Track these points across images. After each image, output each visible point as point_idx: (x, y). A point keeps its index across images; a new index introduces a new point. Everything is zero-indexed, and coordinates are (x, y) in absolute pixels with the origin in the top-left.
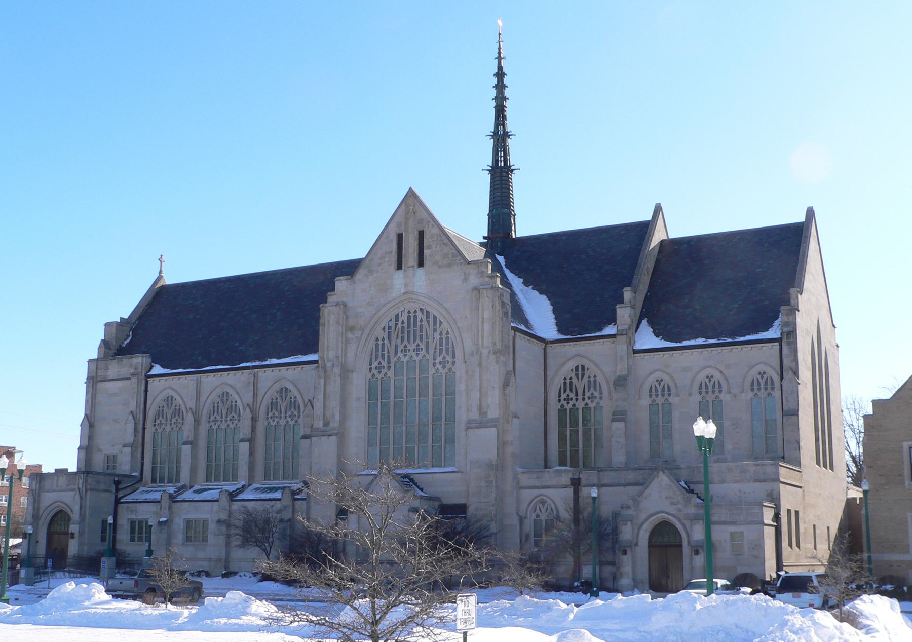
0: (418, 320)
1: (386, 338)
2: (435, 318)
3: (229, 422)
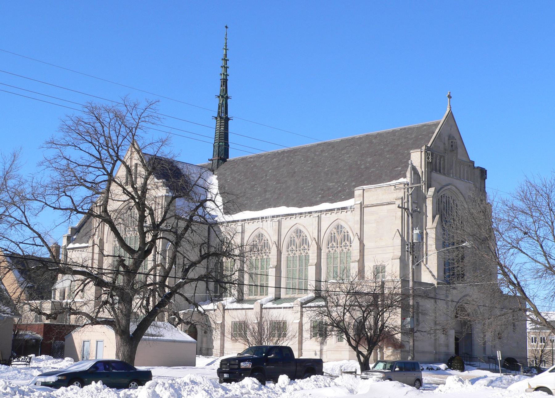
3: (343, 248)
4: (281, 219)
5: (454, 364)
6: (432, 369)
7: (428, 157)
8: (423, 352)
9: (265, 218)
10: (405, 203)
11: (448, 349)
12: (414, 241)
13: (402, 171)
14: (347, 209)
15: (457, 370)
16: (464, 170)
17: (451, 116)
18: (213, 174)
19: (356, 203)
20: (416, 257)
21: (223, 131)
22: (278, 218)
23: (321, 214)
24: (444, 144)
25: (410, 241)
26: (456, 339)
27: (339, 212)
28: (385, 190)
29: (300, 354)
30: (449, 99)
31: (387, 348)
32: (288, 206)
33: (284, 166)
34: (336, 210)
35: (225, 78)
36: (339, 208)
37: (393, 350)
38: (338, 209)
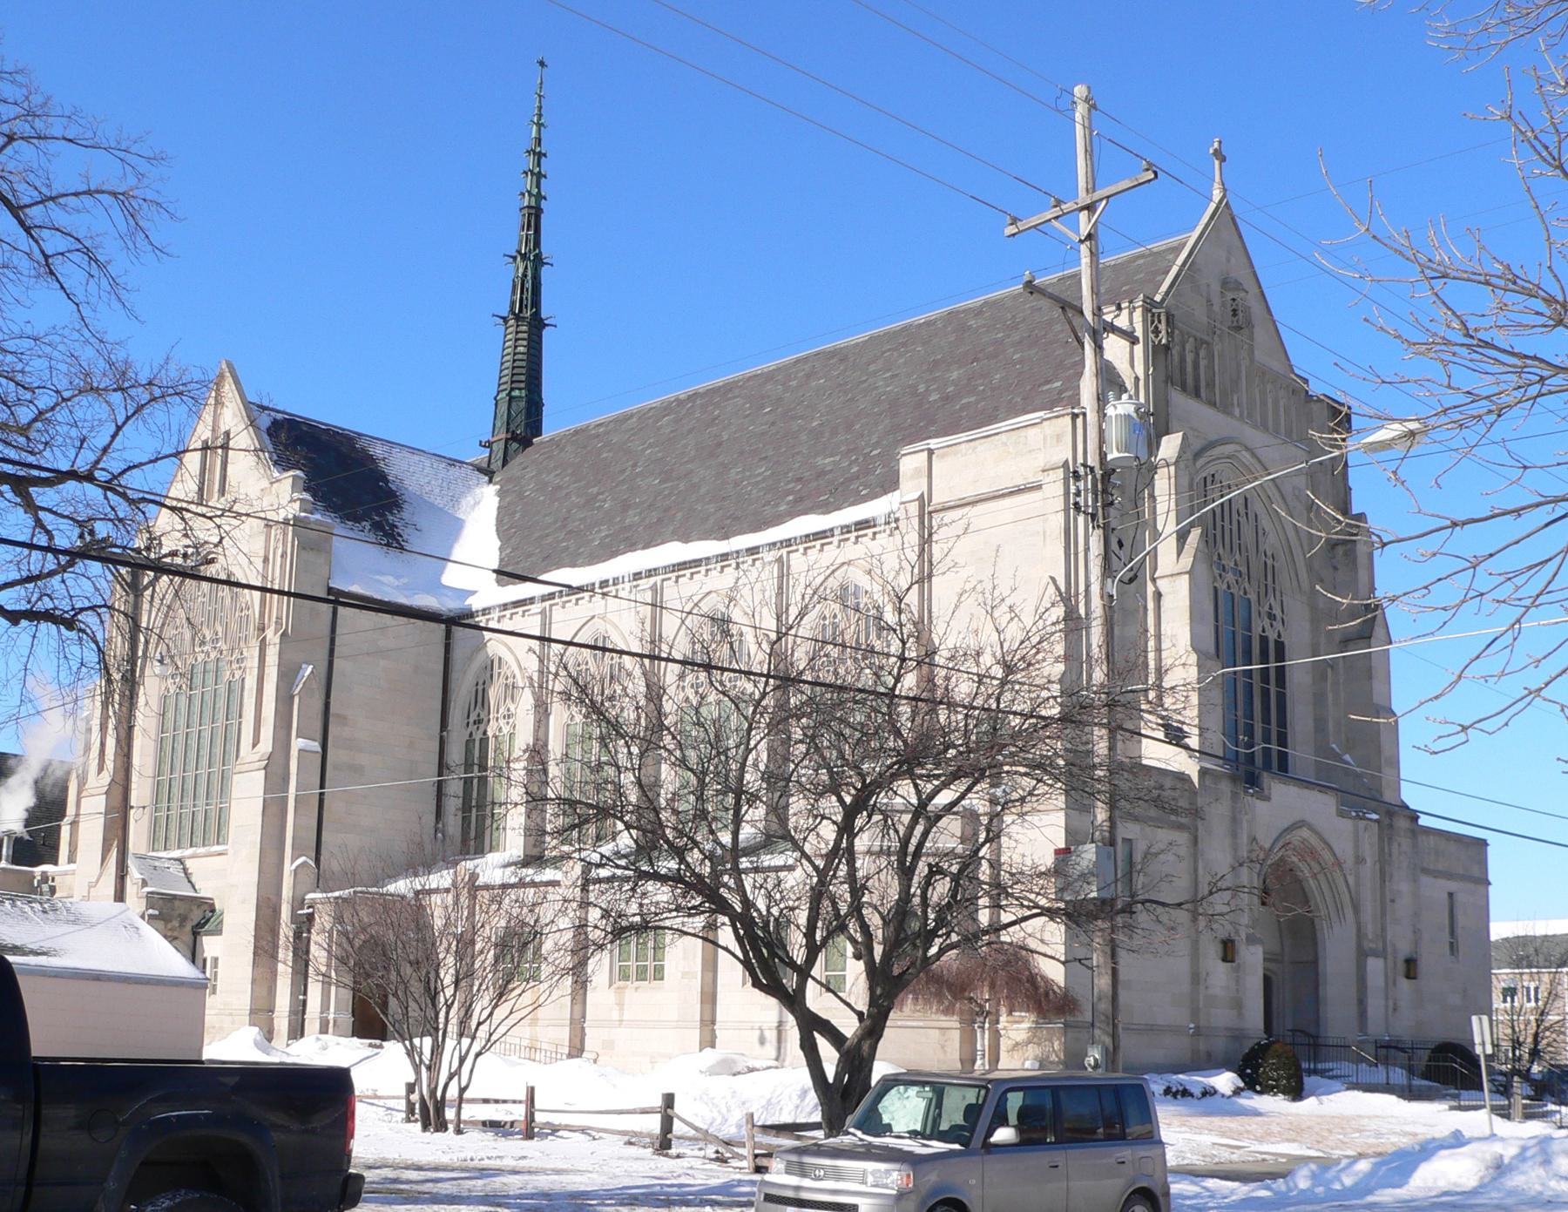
4: (663, 580)
5: (1264, 1072)
6: (1185, 1093)
7: (1156, 327)
8: (1151, 1029)
9: (611, 582)
11: (1240, 1015)
12: (1110, 457)
13: (1066, 390)
14: (875, 526)
15: (1275, 1094)
16: (1276, 402)
17: (1226, 217)
18: (490, 481)
19: (904, 500)
20: (1121, 544)
21: (525, 357)
22: (652, 580)
23: (789, 553)
24: (1209, 302)
25: (1093, 460)
26: (1267, 981)
27: (848, 539)
28: (1005, 444)
29: (709, 1039)
30: (1217, 163)
31: (1010, 1013)
32: (686, 539)
33: (690, 431)
34: (837, 532)
35: (533, 204)
36: (847, 526)
37: (1037, 1023)
38: (846, 529)
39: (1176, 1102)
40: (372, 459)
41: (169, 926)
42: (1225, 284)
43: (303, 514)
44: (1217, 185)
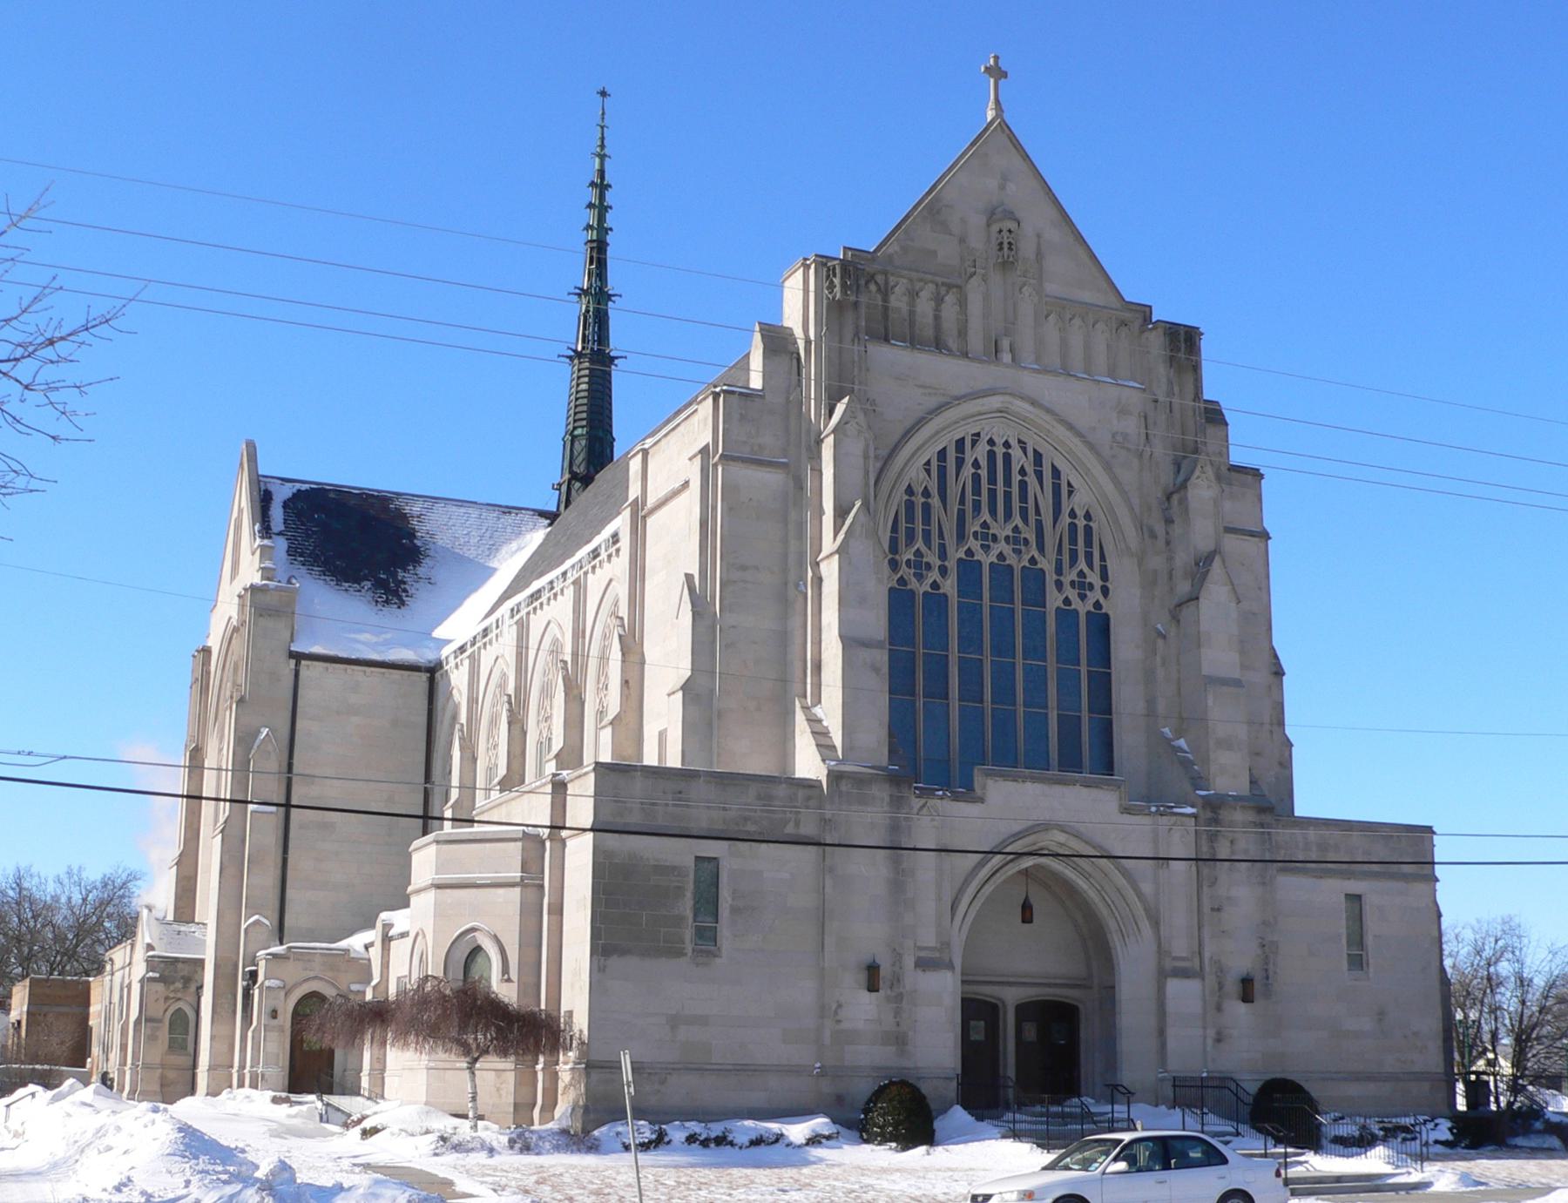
0: (1015, 468)
1: (934, 491)
2: (1056, 473)
6: (721, 1141)
7: (832, 282)
10: (715, 465)
39: (707, 1151)
40: (404, 517)
41: (172, 988)
42: (992, 215)
43: (264, 582)
44: (991, 104)
